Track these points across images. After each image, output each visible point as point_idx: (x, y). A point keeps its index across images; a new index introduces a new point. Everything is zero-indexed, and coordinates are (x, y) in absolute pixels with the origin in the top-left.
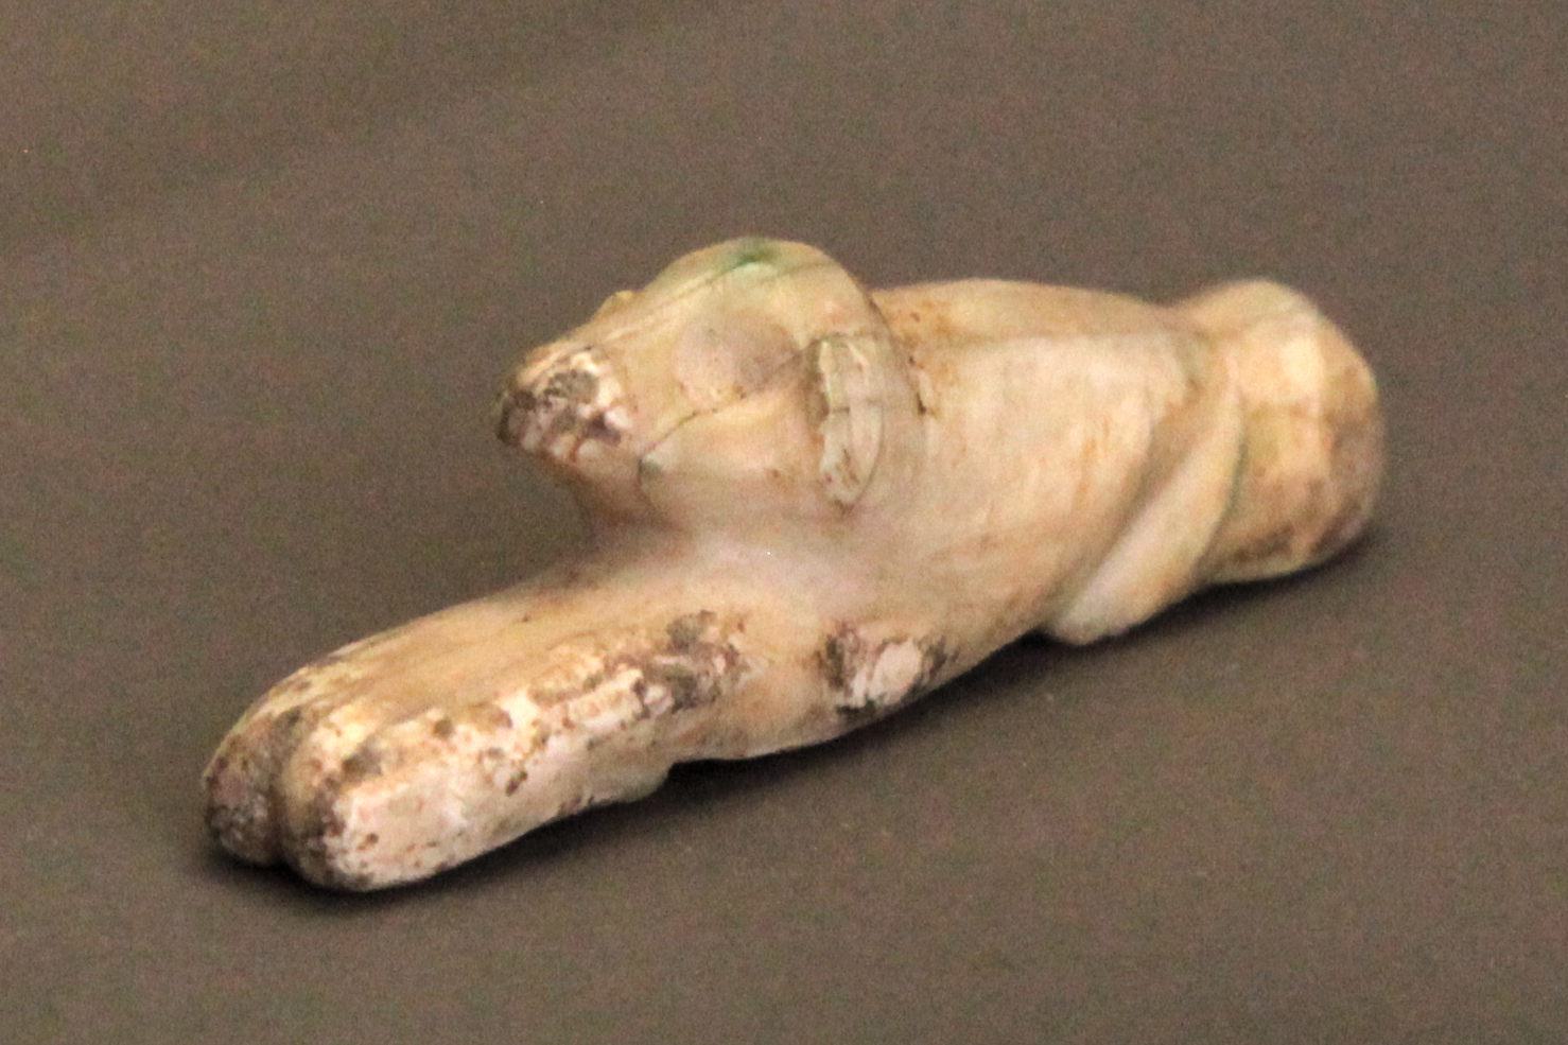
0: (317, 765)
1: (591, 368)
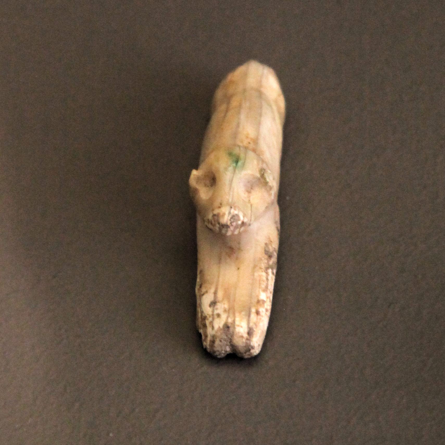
0: (242, 337)
1: (236, 212)
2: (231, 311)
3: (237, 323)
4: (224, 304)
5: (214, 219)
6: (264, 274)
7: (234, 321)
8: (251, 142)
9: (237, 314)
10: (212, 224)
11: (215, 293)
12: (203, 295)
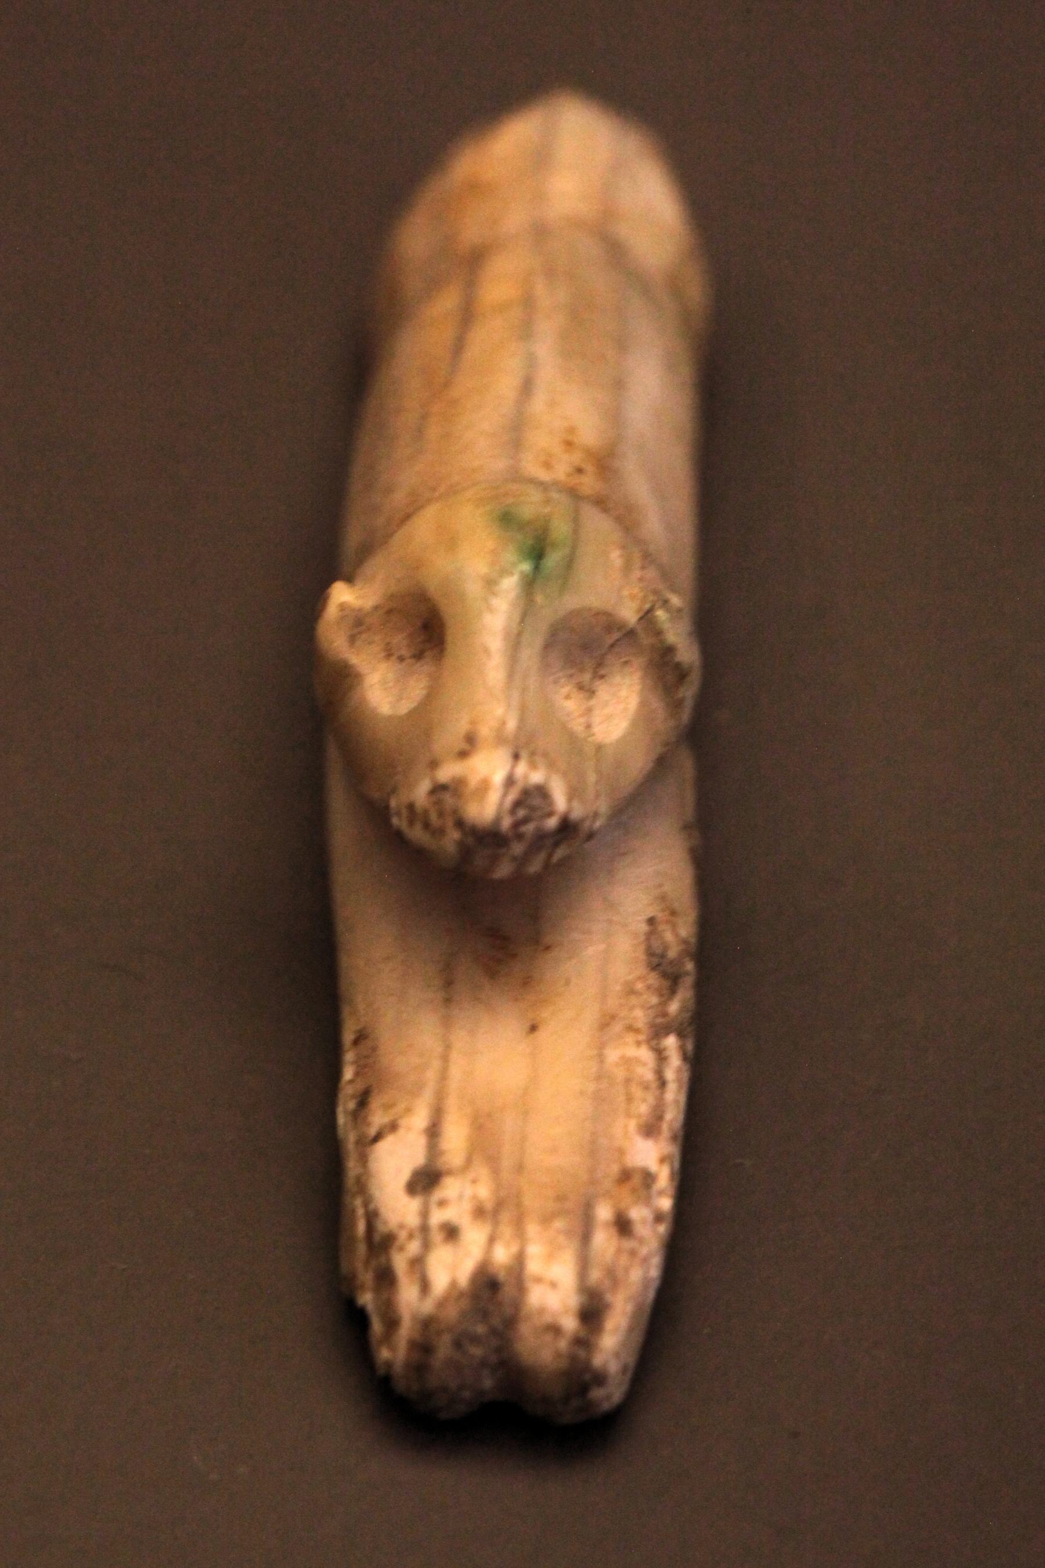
0: (555, 1329)
1: (537, 777)
2: (505, 1216)
3: (534, 1266)
4: (474, 1182)
5: (438, 803)
6: (645, 1054)
7: (520, 1259)
8: (589, 468)
9: (532, 1229)
10: (427, 826)
11: (433, 1132)
12: (378, 1138)
